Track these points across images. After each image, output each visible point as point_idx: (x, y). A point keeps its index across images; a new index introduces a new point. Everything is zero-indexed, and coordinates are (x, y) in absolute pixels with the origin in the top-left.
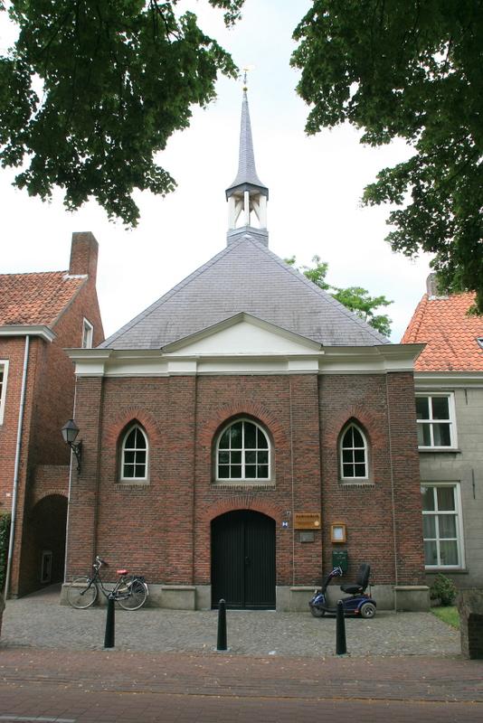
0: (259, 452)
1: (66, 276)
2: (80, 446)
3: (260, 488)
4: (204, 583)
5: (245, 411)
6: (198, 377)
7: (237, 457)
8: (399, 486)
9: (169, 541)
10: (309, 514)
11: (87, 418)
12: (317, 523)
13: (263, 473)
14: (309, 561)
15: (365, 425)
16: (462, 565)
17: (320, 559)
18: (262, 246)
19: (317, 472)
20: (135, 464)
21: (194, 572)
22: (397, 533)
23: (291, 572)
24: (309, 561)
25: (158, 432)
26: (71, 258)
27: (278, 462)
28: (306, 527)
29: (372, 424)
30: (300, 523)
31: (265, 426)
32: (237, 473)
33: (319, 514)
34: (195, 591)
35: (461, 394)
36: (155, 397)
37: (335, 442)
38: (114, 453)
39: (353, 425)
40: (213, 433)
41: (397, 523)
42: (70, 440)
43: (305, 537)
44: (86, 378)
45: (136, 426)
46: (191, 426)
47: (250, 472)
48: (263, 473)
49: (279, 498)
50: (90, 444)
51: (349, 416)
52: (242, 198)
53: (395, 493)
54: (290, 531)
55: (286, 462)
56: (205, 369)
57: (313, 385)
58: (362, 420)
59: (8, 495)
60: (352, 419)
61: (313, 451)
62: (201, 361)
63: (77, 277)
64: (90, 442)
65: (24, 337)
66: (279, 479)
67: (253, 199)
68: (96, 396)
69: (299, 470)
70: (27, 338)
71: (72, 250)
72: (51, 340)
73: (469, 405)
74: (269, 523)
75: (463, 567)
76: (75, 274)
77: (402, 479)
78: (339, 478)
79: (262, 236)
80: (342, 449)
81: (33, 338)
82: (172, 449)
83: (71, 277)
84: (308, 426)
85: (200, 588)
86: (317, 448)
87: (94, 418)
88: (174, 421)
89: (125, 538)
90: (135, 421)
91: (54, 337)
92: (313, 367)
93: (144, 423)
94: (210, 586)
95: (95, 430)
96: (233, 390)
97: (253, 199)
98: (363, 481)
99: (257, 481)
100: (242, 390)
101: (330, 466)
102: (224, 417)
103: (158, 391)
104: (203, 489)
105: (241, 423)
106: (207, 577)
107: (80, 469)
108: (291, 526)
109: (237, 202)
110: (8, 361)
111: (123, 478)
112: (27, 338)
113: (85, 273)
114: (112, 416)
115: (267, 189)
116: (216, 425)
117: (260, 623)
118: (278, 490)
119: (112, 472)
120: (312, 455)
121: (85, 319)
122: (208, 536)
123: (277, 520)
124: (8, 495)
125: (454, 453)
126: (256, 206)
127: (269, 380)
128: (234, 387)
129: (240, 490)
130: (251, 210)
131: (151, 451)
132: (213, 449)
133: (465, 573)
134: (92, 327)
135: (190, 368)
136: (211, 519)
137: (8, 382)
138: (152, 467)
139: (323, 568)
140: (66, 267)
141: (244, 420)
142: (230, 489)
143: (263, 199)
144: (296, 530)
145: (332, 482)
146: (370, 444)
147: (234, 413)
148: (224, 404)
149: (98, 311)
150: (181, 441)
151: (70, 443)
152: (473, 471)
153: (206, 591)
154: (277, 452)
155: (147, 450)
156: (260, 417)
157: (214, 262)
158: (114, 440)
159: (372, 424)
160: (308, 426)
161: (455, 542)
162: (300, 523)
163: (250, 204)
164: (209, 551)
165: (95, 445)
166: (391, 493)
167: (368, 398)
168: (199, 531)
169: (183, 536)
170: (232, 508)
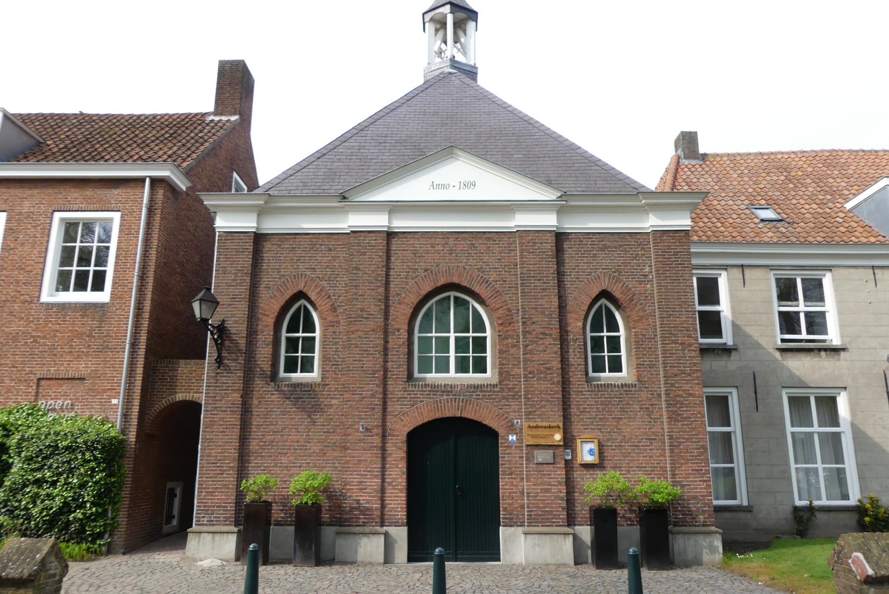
0: (474, 338)
1: (212, 118)
2: (221, 329)
3: (476, 387)
4: (396, 525)
5: (456, 280)
6: (390, 235)
7: (443, 344)
8: (672, 385)
9: (347, 463)
10: (547, 424)
11: (232, 289)
12: (558, 437)
13: (480, 367)
14: (547, 491)
15: (621, 301)
16: (742, 499)
17: (563, 488)
18: (471, 82)
19: (556, 364)
20: (300, 354)
21: (383, 507)
22: (672, 451)
23: (523, 507)
24: (547, 491)
25: (334, 309)
26: (218, 94)
27: (501, 351)
28: (543, 442)
29: (631, 300)
30: (533, 437)
31: (482, 302)
32: (443, 367)
33: (561, 424)
34: (386, 534)
35: (737, 273)
36: (329, 261)
37: (580, 324)
38: (270, 338)
39: (603, 301)
40: (411, 311)
41: (671, 437)
42: (204, 316)
43: (542, 456)
44: (230, 235)
45: (303, 302)
46: (380, 300)
47: (462, 367)
48: (480, 367)
49: (504, 402)
50: (237, 327)
51: (600, 289)
52: (444, 25)
53: (667, 394)
54: (520, 448)
55: (512, 351)
56: (402, 223)
57: (549, 245)
58: (617, 294)
59: (115, 401)
60: (605, 294)
61: (551, 335)
62: (395, 208)
63: (224, 118)
64: (235, 322)
65: (142, 180)
66: (503, 374)
67: (459, 26)
68: (246, 260)
69: (532, 361)
70: (148, 180)
71: (219, 83)
72: (184, 188)
73: (746, 288)
74: (491, 435)
75: (745, 503)
76: (221, 114)
77: (676, 375)
78: (587, 374)
79: (471, 73)
80: (589, 334)
81: (155, 181)
82: (353, 332)
83: (217, 118)
84: (541, 302)
85: (392, 530)
86: (555, 333)
87: (243, 290)
88: (356, 294)
89: (284, 460)
90: (300, 295)
91: (189, 184)
92: (548, 221)
93: (313, 297)
94: (405, 529)
95: (243, 307)
96: (438, 252)
97: (459, 26)
98: (619, 378)
99: (472, 377)
100: (451, 252)
101: (574, 358)
102: (427, 288)
103: (333, 253)
104: (396, 388)
105: (449, 297)
106: (401, 514)
107: (219, 361)
108: (520, 440)
109: (437, 30)
110: (119, 213)
111: (282, 374)
112: (148, 180)
113: (235, 114)
114: (268, 288)
115: (476, 13)
116: (414, 300)
117: (485, 584)
118: (502, 390)
119: (267, 368)
120: (548, 341)
121: (235, 175)
122: (404, 455)
123: (501, 432)
124: (115, 401)
125: (726, 351)
126: (461, 33)
127: (489, 239)
128: (440, 248)
129: (448, 389)
130: (456, 42)
131: (324, 336)
132: (410, 333)
133: (748, 509)
134: (245, 188)
135: (378, 221)
136: (407, 429)
137: (119, 242)
138: (325, 358)
139: (568, 501)
140: (211, 109)
141: (453, 294)
142: (435, 388)
143: (471, 25)
144: (528, 445)
145: (576, 377)
146: (628, 328)
147: (439, 284)
148: (426, 270)
149: (254, 169)
150: (365, 321)
151: (205, 321)
152: (754, 372)
153: (400, 534)
154: (501, 338)
155: (317, 334)
156: (477, 289)
157: (408, 99)
158: (270, 320)
159: (631, 300)
160: (541, 302)
161: (732, 469)
162: (533, 437)
163: (455, 33)
164: (405, 477)
165: (243, 328)
166: (660, 395)
167: (626, 264)
168: (390, 447)
169: (368, 456)
170: (438, 415)
